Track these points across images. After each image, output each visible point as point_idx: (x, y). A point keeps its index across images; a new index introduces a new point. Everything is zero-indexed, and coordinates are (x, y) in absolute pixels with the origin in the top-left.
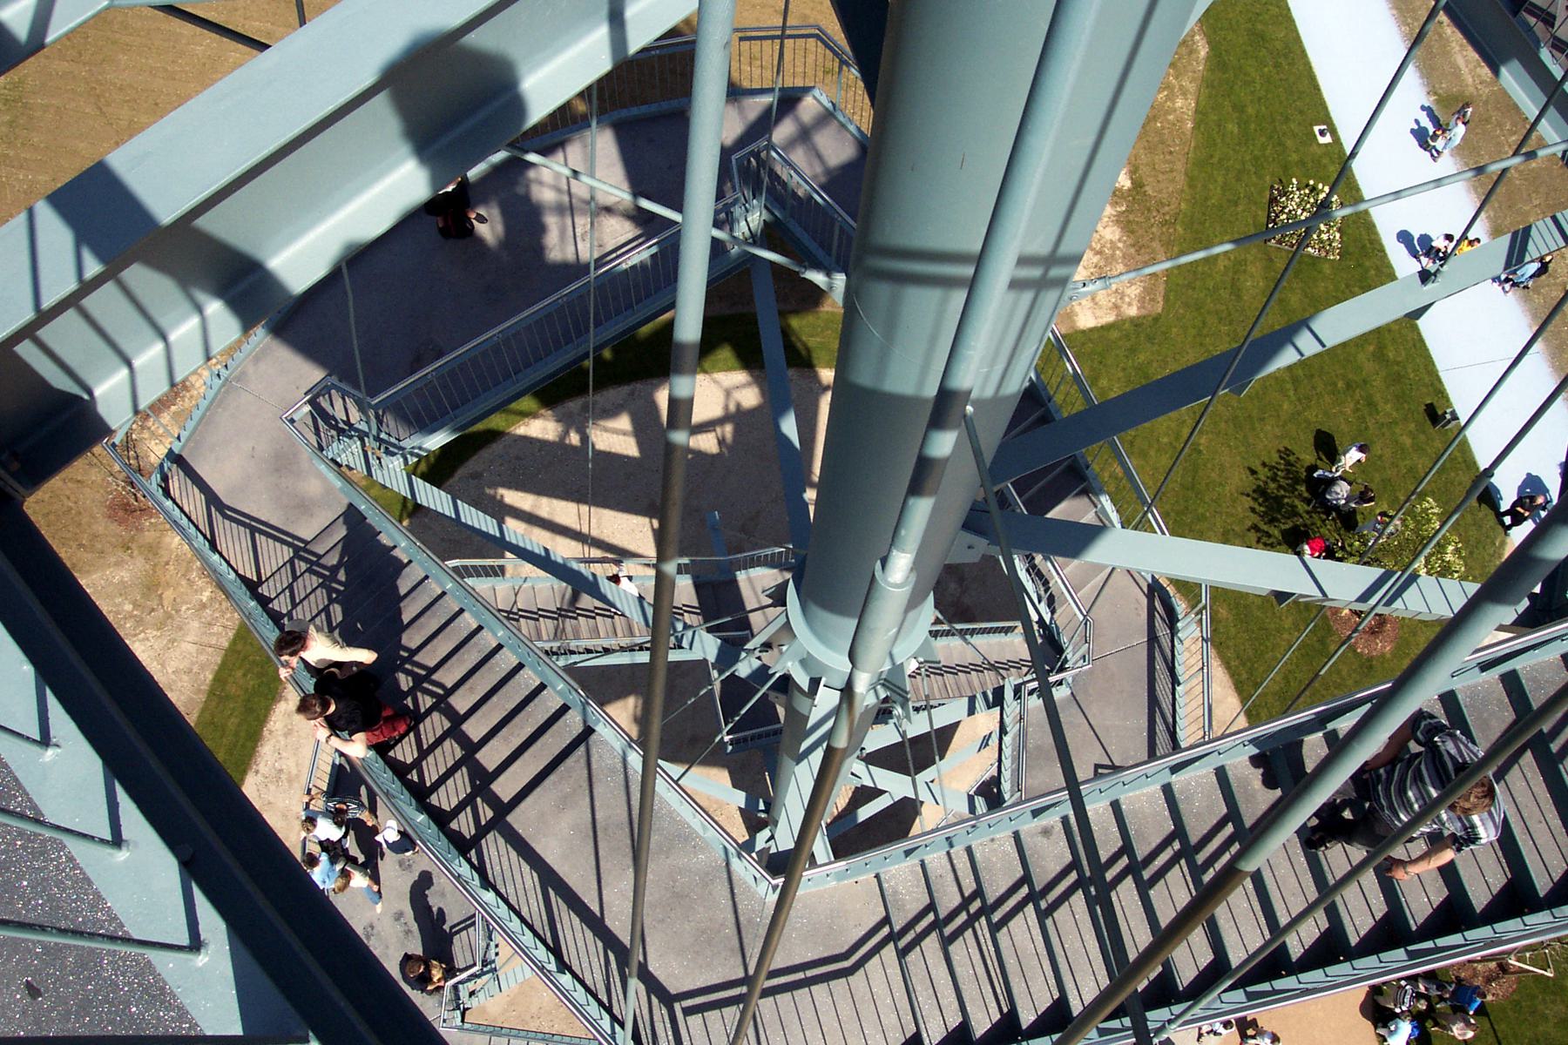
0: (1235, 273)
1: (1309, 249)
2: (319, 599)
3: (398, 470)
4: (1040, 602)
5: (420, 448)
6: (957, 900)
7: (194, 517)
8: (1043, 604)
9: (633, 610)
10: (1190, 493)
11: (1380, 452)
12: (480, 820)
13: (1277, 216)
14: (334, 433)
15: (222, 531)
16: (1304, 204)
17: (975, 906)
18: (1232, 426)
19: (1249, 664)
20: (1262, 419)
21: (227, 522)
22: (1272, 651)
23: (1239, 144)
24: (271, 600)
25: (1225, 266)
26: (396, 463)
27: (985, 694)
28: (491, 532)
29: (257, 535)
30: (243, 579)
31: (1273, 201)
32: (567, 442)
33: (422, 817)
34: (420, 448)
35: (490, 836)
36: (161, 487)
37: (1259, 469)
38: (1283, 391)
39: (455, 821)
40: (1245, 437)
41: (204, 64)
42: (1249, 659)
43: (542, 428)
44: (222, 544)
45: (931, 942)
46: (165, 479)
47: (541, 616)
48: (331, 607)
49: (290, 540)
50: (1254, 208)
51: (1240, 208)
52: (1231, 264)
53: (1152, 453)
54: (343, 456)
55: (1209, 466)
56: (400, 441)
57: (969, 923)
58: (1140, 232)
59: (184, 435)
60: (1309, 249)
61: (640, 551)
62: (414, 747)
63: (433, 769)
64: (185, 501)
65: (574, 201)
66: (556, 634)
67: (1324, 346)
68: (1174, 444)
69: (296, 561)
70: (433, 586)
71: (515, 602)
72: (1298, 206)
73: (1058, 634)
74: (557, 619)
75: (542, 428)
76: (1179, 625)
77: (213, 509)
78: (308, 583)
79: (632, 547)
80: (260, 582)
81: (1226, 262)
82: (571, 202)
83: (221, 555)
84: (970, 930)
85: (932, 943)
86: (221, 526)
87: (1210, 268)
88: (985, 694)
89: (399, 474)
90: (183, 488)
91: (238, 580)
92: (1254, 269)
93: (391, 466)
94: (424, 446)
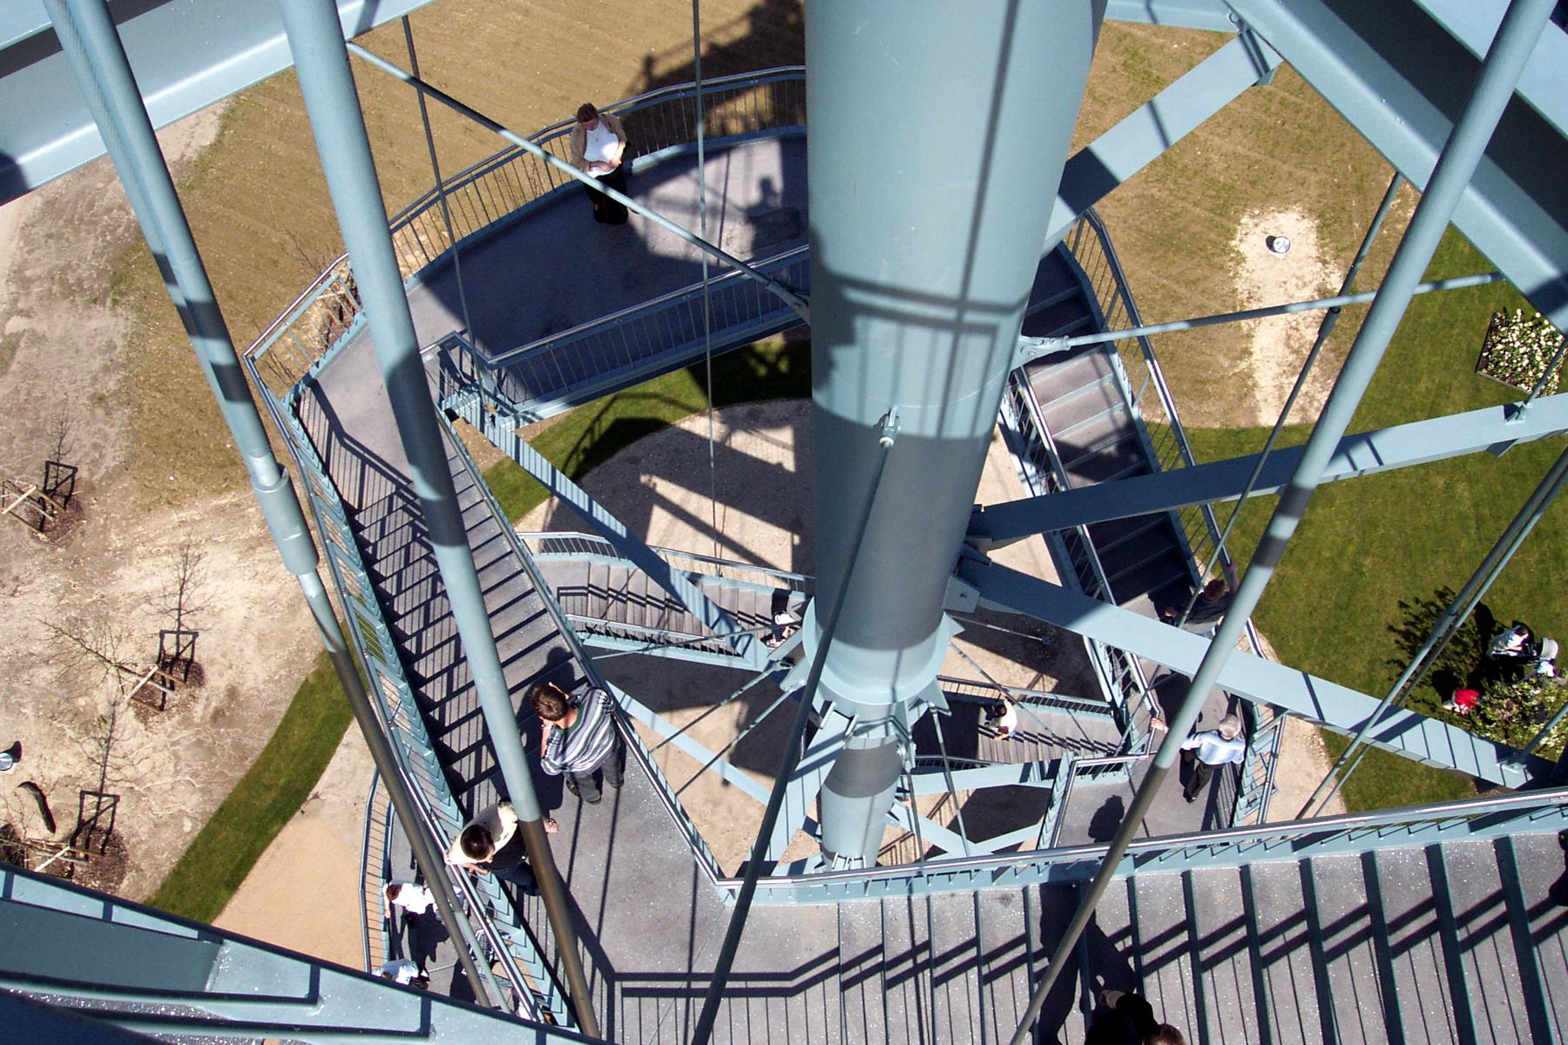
0: (1438, 396)
1: (1523, 385)
2: (405, 535)
3: (509, 431)
4: (1113, 682)
5: (533, 414)
6: (906, 946)
7: (315, 440)
8: (1116, 685)
9: (697, 608)
10: (1343, 614)
11: (1558, 610)
12: (480, 765)
13: (1494, 345)
14: (457, 385)
15: (336, 457)
16: (1526, 337)
17: (923, 957)
18: (1402, 552)
19: (1370, 802)
20: (1434, 552)
21: (343, 448)
22: (1398, 793)
23: (1467, 265)
24: (363, 528)
25: (1427, 388)
26: (508, 424)
27: (1041, 764)
28: (581, 506)
29: (367, 466)
30: (345, 504)
31: (1493, 329)
32: (727, 444)
33: (430, 752)
34: (533, 414)
35: (484, 784)
36: (293, 406)
37: (1411, 603)
38: (1464, 528)
39: (458, 763)
40: (1414, 567)
41: (463, 31)
42: (1371, 797)
43: (705, 426)
44: (333, 470)
45: (874, 983)
46: (298, 399)
47: (648, 602)
48: (412, 545)
49: (395, 477)
50: (1470, 333)
51: (1456, 331)
52: (1435, 386)
53: (1311, 565)
54: (462, 408)
55: (1369, 589)
56: (514, 403)
57: (914, 972)
58: (1344, 338)
59: (323, 362)
60: (1523, 385)
61: (776, 563)
62: (445, 688)
63: (454, 712)
64: (311, 422)
65: (727, 206)
66: (659, 623)
67: (1380, 463)
68: (1336, 559)
69: (395, 497)
70: (505, 542)
71: (627, 585)
72: (1519, 339)
73: (1128, 718)
74: (663, 609)
75: (705, 426)
76: (1256, 736)
77: (334, 435)
78: (399, 518)
79: (768, 558)
80: (360, 510)
81: (1430, 385)
82: (724, 207)
83: (331, 478)
84: (912, 979)
85: (874, 983)
86: (337, 452)
87: (1411, 388)
88: (1041, 764)
89: (508, 436)
90: (312, 411)
91: (340, 505)
92: (1457, 397)
93: (503, 426)
94: (538, 413)
